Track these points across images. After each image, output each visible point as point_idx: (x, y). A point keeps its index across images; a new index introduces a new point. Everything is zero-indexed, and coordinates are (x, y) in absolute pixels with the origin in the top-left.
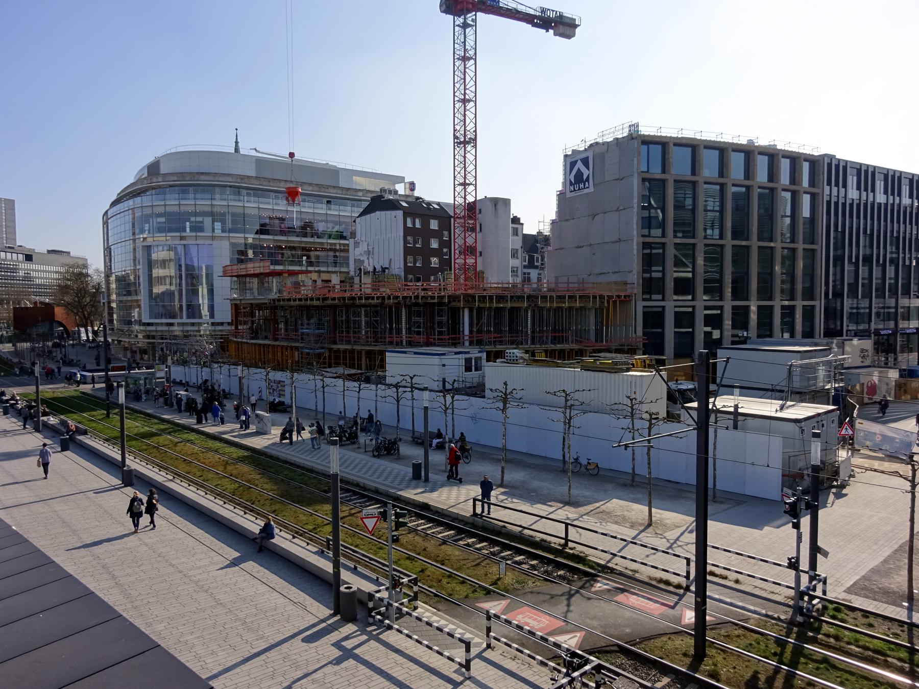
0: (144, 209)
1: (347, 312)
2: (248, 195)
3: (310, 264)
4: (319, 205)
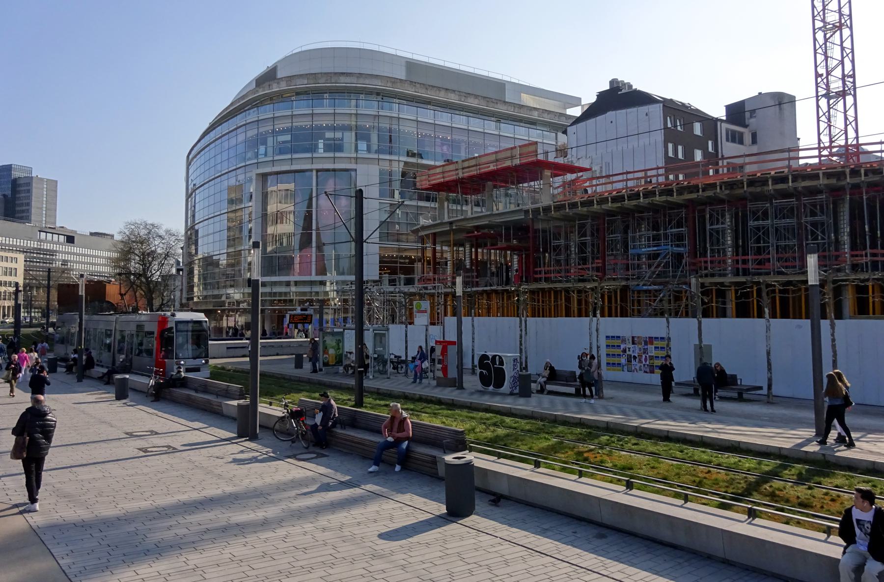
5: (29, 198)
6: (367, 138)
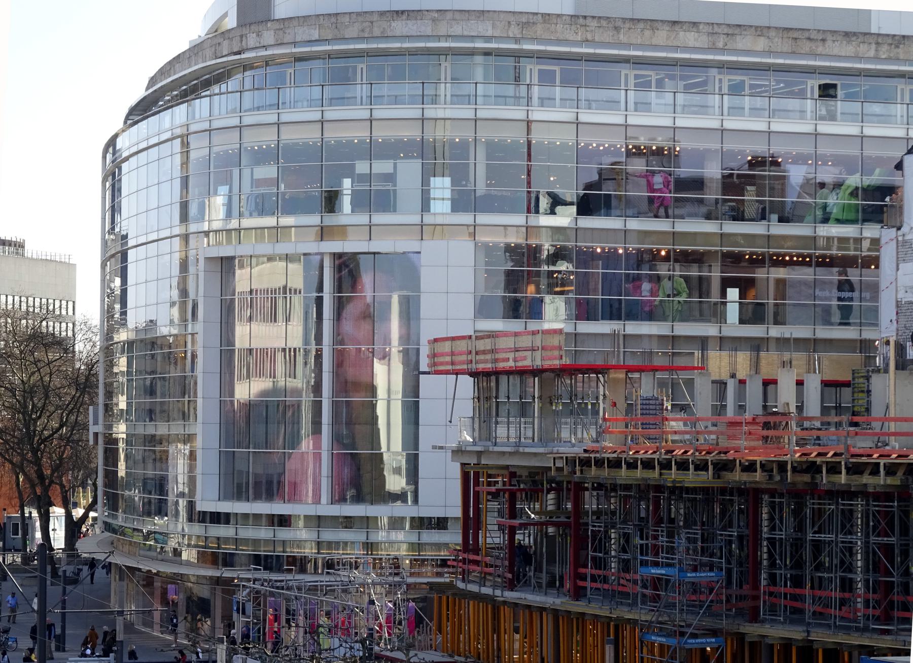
0: (217, 138)
1: (798, 513)
2: (546, 79)
3: (753, 314)
4: (793, 104)
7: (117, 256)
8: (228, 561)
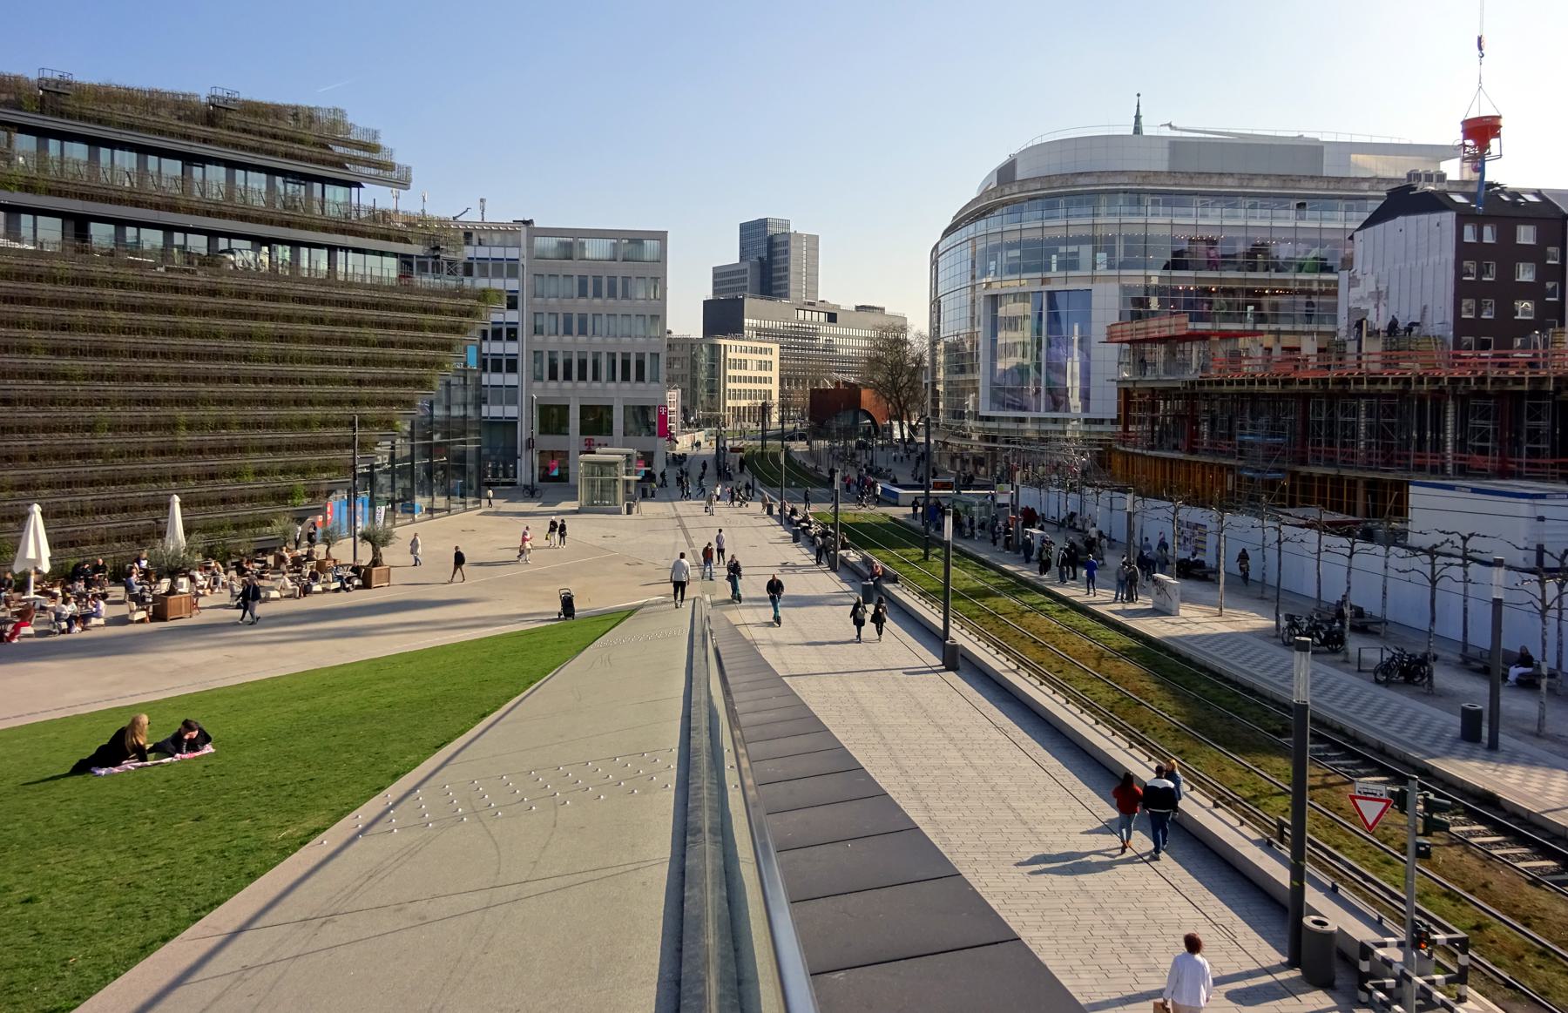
1: (1330, 406)
2: (1155, 203)
3: (1260, 318)
4: (1283, 213)
5: (786, 260)
6: (1111, 252)
7: (936, 304)
8: (994, 439)
